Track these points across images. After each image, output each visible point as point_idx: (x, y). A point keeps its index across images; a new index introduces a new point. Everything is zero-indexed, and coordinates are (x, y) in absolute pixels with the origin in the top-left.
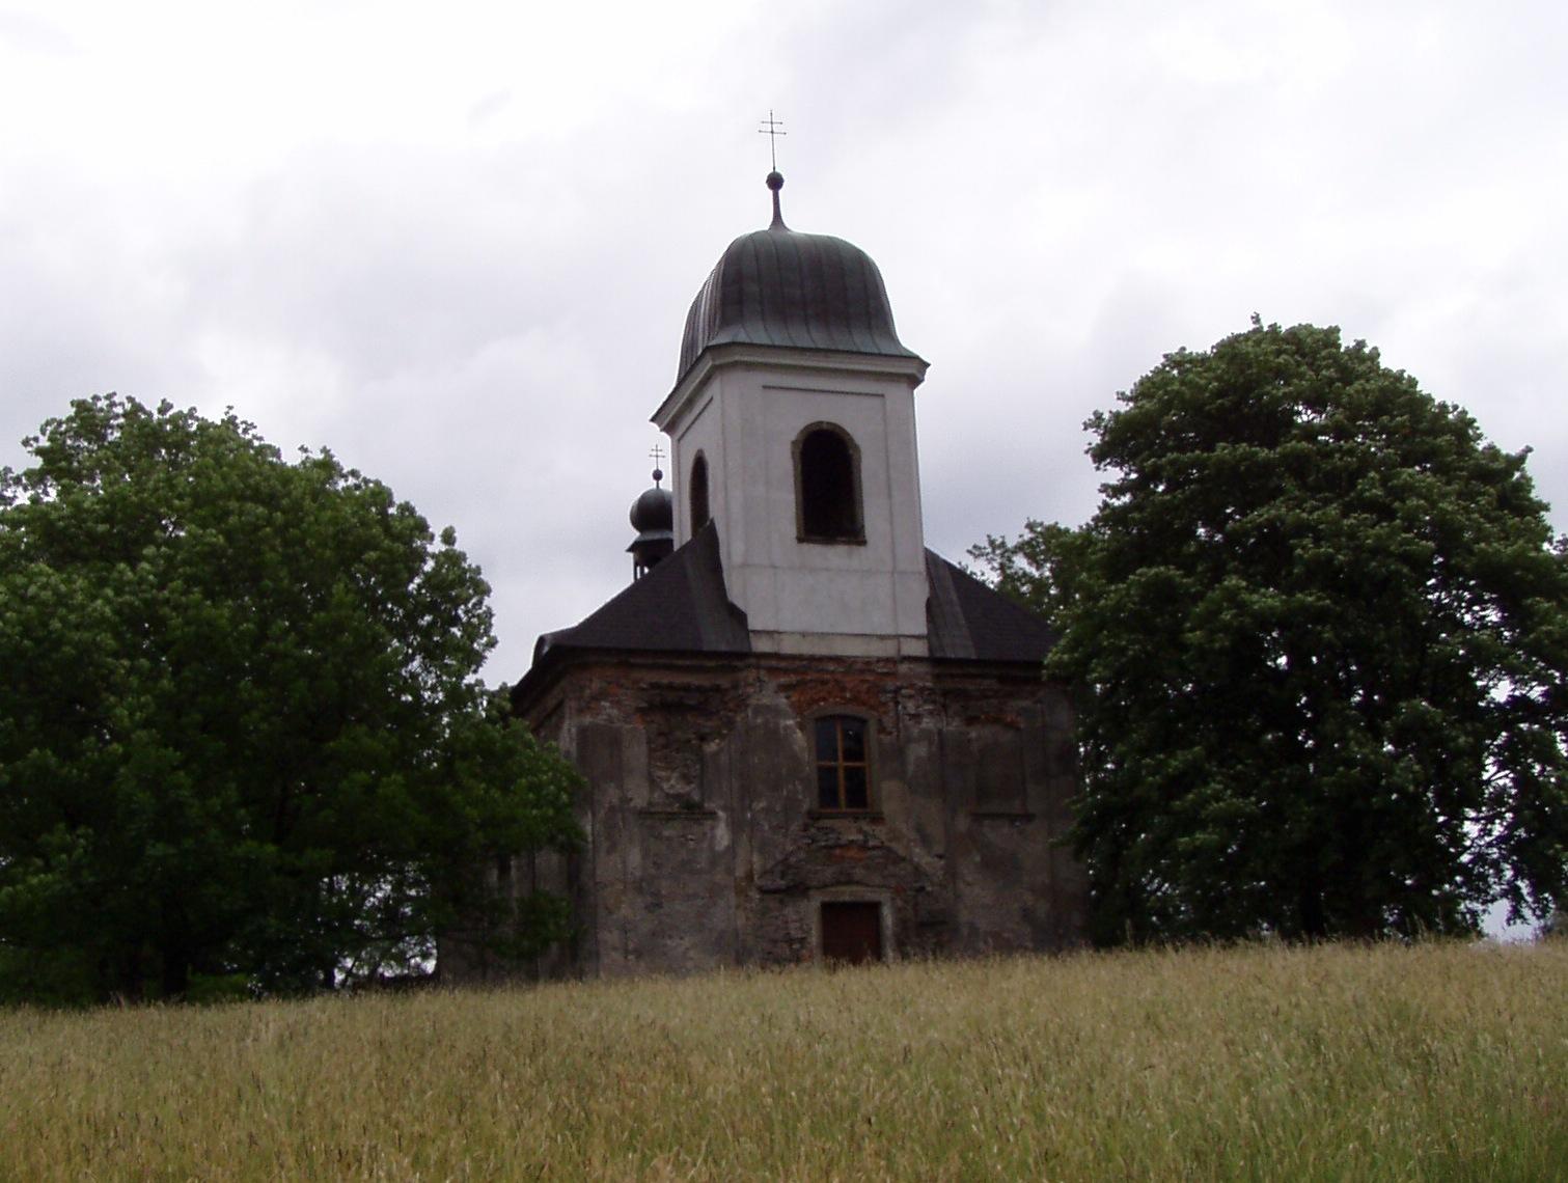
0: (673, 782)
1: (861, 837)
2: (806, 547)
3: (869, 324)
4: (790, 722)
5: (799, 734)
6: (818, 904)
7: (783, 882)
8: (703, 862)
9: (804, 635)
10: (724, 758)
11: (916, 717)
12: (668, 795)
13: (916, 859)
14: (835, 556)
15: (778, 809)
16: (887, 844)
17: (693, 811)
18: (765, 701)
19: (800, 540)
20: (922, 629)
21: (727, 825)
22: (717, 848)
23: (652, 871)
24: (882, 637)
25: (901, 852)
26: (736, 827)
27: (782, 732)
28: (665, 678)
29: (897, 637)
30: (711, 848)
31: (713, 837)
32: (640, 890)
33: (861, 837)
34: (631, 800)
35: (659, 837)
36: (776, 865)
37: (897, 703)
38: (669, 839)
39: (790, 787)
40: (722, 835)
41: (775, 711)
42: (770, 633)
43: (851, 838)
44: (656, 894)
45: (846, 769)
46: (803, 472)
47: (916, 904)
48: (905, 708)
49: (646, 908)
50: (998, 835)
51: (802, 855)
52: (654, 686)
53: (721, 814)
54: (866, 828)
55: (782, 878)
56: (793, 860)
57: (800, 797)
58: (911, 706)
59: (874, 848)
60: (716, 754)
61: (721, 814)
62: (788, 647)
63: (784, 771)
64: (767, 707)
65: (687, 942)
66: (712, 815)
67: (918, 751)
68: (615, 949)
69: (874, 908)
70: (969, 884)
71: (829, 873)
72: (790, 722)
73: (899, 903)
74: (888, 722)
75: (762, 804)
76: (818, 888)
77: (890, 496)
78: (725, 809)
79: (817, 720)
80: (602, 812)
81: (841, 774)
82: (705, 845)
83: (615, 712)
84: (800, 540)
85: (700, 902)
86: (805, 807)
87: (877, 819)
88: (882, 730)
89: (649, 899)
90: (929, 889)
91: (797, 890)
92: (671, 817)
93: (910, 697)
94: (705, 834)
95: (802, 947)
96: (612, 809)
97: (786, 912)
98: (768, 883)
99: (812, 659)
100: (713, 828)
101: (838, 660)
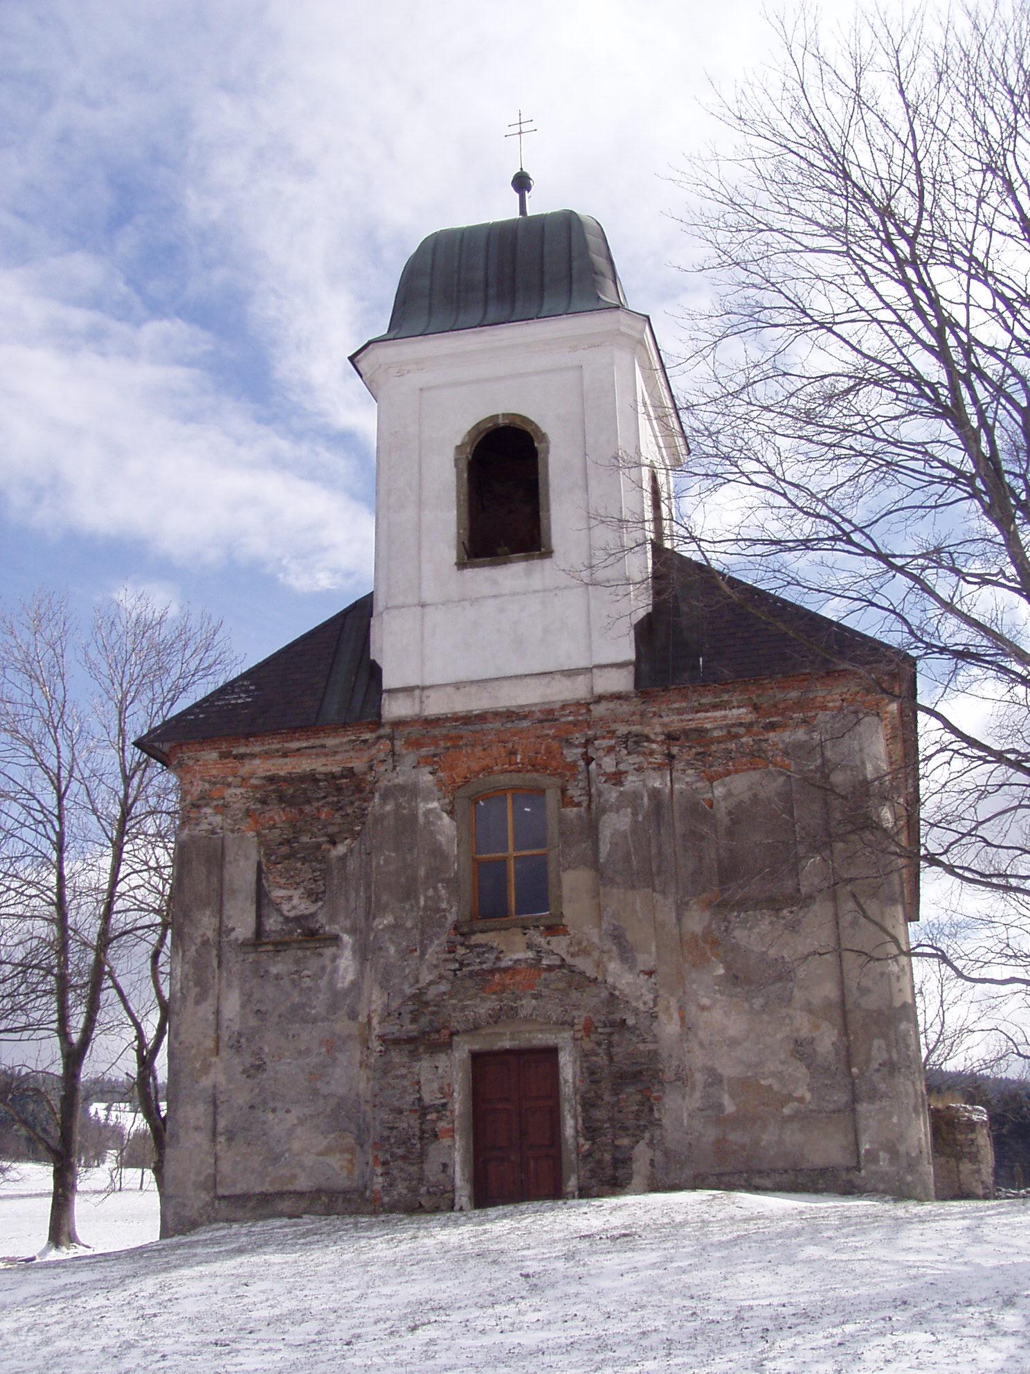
0: (295, 901)
1: (530, 954)
2: (469, 573)
3: (570, 290)
4: (434, 805)
5: (446, 819)
6: (465, 1055)
7: (414, 1027)
8: (319, 1005)
9: (458, 685)
10: (352, 864)
11: (617, 778)
12: (287, 920)
13: (610, 980)
14: (512, 576)
15: (409, 924)
16: (569, 960)
17: (311, 936)
18: (400, 780)
19: (461, 565)
20: (630, 654)
21: (354, 952)
22: (340, 985)
23: (253, 1022)
24: (570, 673)
25: (591, 972)
26: (364, 953)
27: (421, 820)
28: (283, 767)
29: (588, 670)
30: (332, 984)
31: (335, 970)
32: (237, 1048)
33: (530, 954)
34: (233, 929)
35: (264, 976)
36: (404, 1003)
37: (589, 760)
38: (278, 977)
39: (431, 893)
40: (346, 965)
41: (412, 791)
42: (408, 690)
43: (516, 957)
44: (258, 1054)
45: (503, 862)
46: (470, 480)
47: (610, 1044)
48: (599, 766)
49: (244, 1071)
50: (756, 935)
51: (444, 987)
52: (272, 779)
53: (346, 938)
54: (542, 941)
55: (413, 1021)
56: (432, 993)
57: (444, 905)
58: (609, 764)
59: (550, 968)
60: (343, 859)
61: (346, 938)
62: (436, 706)
63: (422, 872)
64: (402, 789)
65: (291, 1119)
66: (335, 940)
67: (616, 824)
68: (197, 1128)
69: (551, 1053)
70: (703, 1008)
71: (484, 1007)
72: (434, 805)
73: (588, 1045)
74: (575, 792)
75: (388, 920)
76: (466, 1032)
77: (586, 489)
78: (353, 931)
79: (166, 743)
80: (193, 948)
81: (511, 865)
82: (323, 983)
83: (218, 819)
84: (549, 554)
85: (315, 1060)
86: (451, 918)
87: (554, 929)
88: (566, 801)
89: (249, 1060)
90: (631, 1021)
91: (430, 1041)
92: (280, 946)
93: (610, 749)
94: (323, 968)
95: (439, 1119)
96: (205, 943)
97: (417, 1066)
98: (392, 1029)
99: (467, 719)
100: (335, 958)
101: (510, 715)
